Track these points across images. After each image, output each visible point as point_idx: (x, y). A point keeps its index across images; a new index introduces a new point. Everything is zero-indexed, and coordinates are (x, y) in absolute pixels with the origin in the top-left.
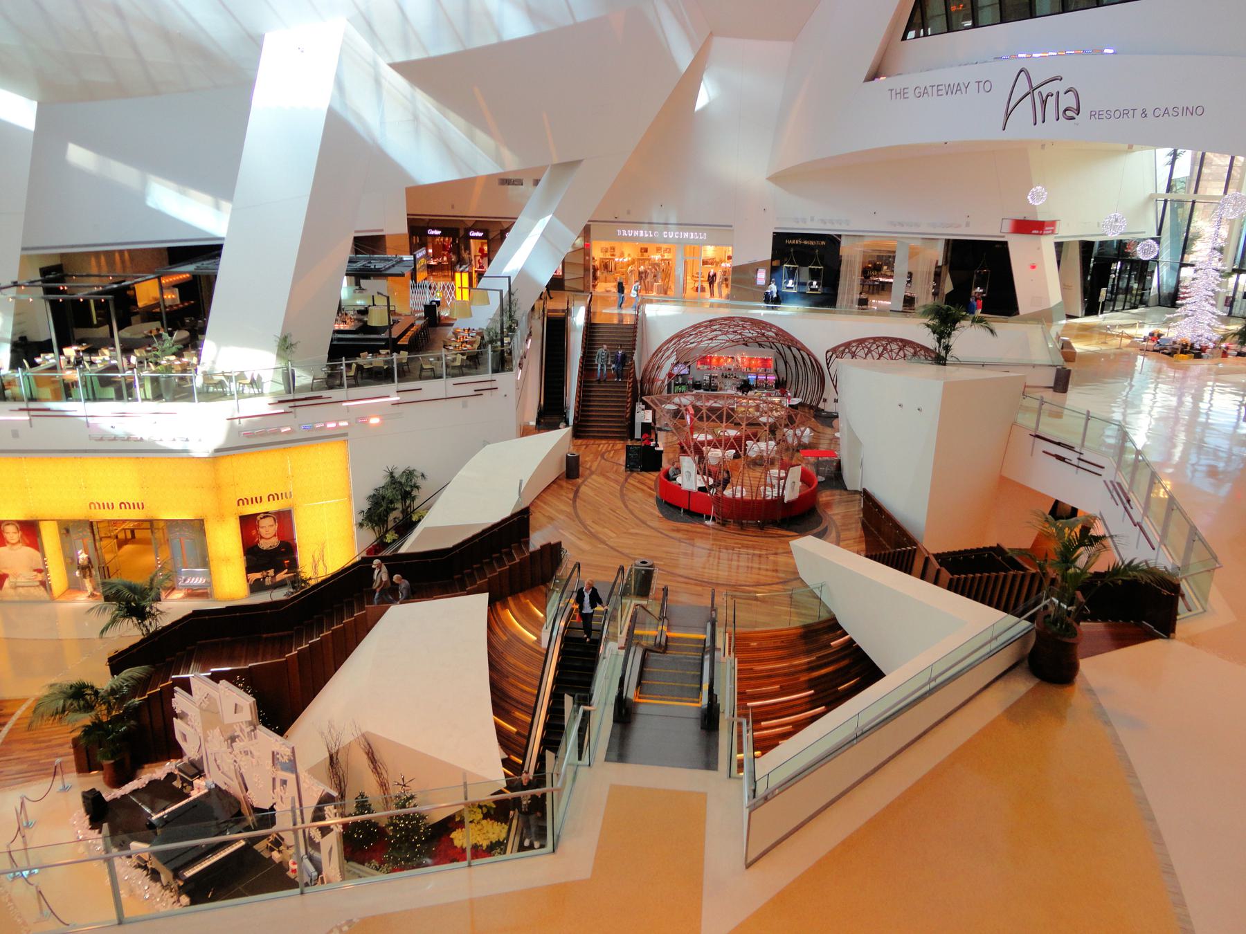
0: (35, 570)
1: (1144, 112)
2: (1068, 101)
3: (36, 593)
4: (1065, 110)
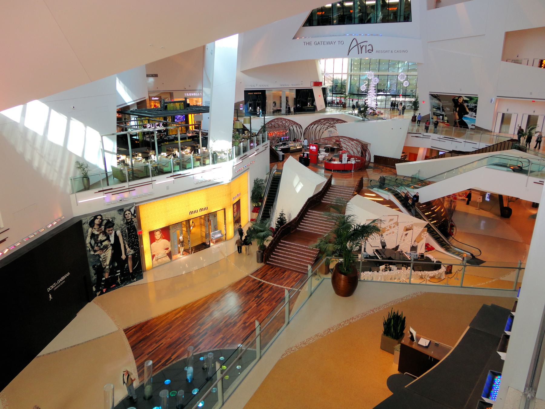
0: (165, 249)
1: (392, 52)
2: (369, 48)
3: (165, 260)
4: (368, 50)
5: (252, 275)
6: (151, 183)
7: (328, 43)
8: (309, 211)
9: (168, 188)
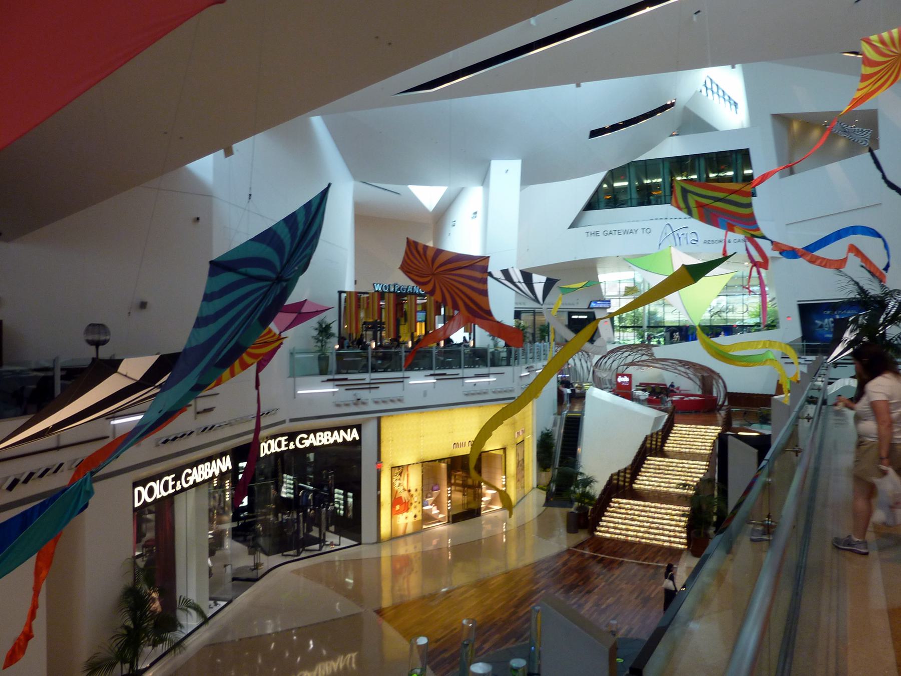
5: (576, 547)
6: (401, 380)
7: (626, 232)
8: (648, 458)
9: (425, 394)
